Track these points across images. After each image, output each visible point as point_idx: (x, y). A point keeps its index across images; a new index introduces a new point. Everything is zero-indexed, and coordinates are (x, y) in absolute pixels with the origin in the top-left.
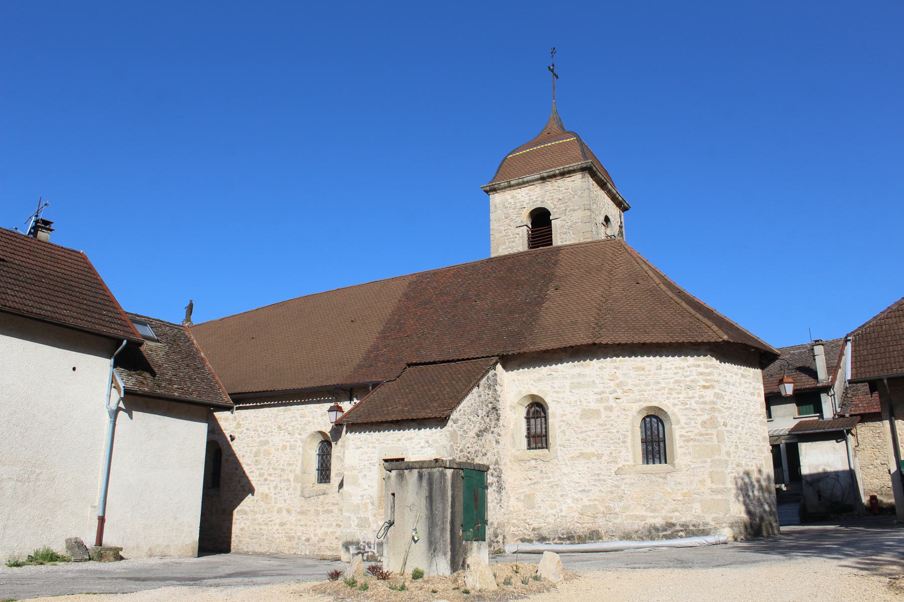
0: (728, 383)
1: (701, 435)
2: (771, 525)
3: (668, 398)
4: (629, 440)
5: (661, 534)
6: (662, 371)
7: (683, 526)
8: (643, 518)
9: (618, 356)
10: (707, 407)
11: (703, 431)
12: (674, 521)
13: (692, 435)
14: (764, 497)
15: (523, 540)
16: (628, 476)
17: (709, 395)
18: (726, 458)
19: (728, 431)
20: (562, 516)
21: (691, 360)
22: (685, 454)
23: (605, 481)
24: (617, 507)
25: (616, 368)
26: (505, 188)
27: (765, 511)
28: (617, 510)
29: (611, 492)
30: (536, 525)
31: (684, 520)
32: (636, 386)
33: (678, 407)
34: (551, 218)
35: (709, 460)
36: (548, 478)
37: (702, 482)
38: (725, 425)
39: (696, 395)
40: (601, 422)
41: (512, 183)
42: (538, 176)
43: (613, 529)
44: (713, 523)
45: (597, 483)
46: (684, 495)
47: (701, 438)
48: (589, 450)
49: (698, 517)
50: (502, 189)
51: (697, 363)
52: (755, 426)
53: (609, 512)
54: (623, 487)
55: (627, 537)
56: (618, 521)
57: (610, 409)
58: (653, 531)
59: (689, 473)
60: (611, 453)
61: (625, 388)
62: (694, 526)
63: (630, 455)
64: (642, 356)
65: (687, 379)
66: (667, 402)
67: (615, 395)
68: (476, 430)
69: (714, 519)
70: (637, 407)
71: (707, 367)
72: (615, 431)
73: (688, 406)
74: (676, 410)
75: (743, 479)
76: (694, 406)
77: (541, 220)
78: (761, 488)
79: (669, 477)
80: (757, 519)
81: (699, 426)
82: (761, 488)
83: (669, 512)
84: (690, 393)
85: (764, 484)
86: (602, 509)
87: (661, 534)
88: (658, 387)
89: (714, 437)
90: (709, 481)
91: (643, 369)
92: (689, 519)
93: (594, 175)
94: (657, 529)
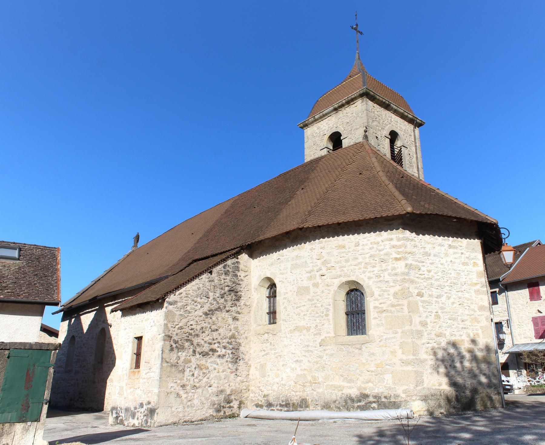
0: (427, 254)
1: (393, 306)
2: (490, 399)
3: (364, 272)
4: (331, 313)
5: (356, 405)
6: (359, 248)
7: (375, 397)
8: (341, 388)
9: (324, 238)
10: (399, 278)
11: (395, 301)
12: (367, 392)
13: (384, 306)
14: (479, 368)
15: (258, 406)
16: (329, 347)
17: (401, 266)
18: (420, 328)
19: (423, 302)
20: (282, 384)
21: (385, 235)
22: (378, 325)
23: (312, 351)
24: (320, 376)
25: (321, 248)
26: (313, 122)
27: (480, 383)
28: (320, 380)
29: (317, 363)
30: (266, 392)
31: (376, 391)
32: (338, 263)
33: (372, 280)
34: (342, 138)
35: (400, 331)
36: (275, 349)
37: (393, 353)
38: (420, 295)
39: (389, 268)
40: (310, 298)
41: (316, 117)
42: (332, 108)
43: (316, 398)
44: (403, 395)
45: (307, 354)
46: (377, 366)
47: (393, 309)
48: (302, 323)
49: (390, 388)
50: (310, 124)
51: (390, 237)
52: (467, 295)
53: (315, 382)
54: (324, 358)
55: (326, 406)
56: (320, 390)
57: (316, 285)
58: (349, 401)
59: (381, 343)
60: (317, 326)
61: (329, 265)
62: (385, 397)
63: (332, 327)
64: (343, 235)
65: (382, 253)
66: (363, 276)
67: (321, 272)
68: (206, 309)
69: (405, 392)
70: (337, 282)
71: (399, 240)
72: (319, 305)
73: (381, 279)
74: (371, 283)
75: (445, 350)
76: (387, 278)
77: (336, 139)
78: (474, 358)
79: (364, 347)
80: (468, 393)
81: (391, 297)
82: (474, 358)
83: (363, 382)
84: (384, 265)
85: (480, 354)
86: (309, 378)
87: (356, 405)
88: (356, 262)
89: (405, 308)
90: (400, 352)
91: (344, 247)
92: (381, 390)
93: (373, 99)
94: (352, 400)
